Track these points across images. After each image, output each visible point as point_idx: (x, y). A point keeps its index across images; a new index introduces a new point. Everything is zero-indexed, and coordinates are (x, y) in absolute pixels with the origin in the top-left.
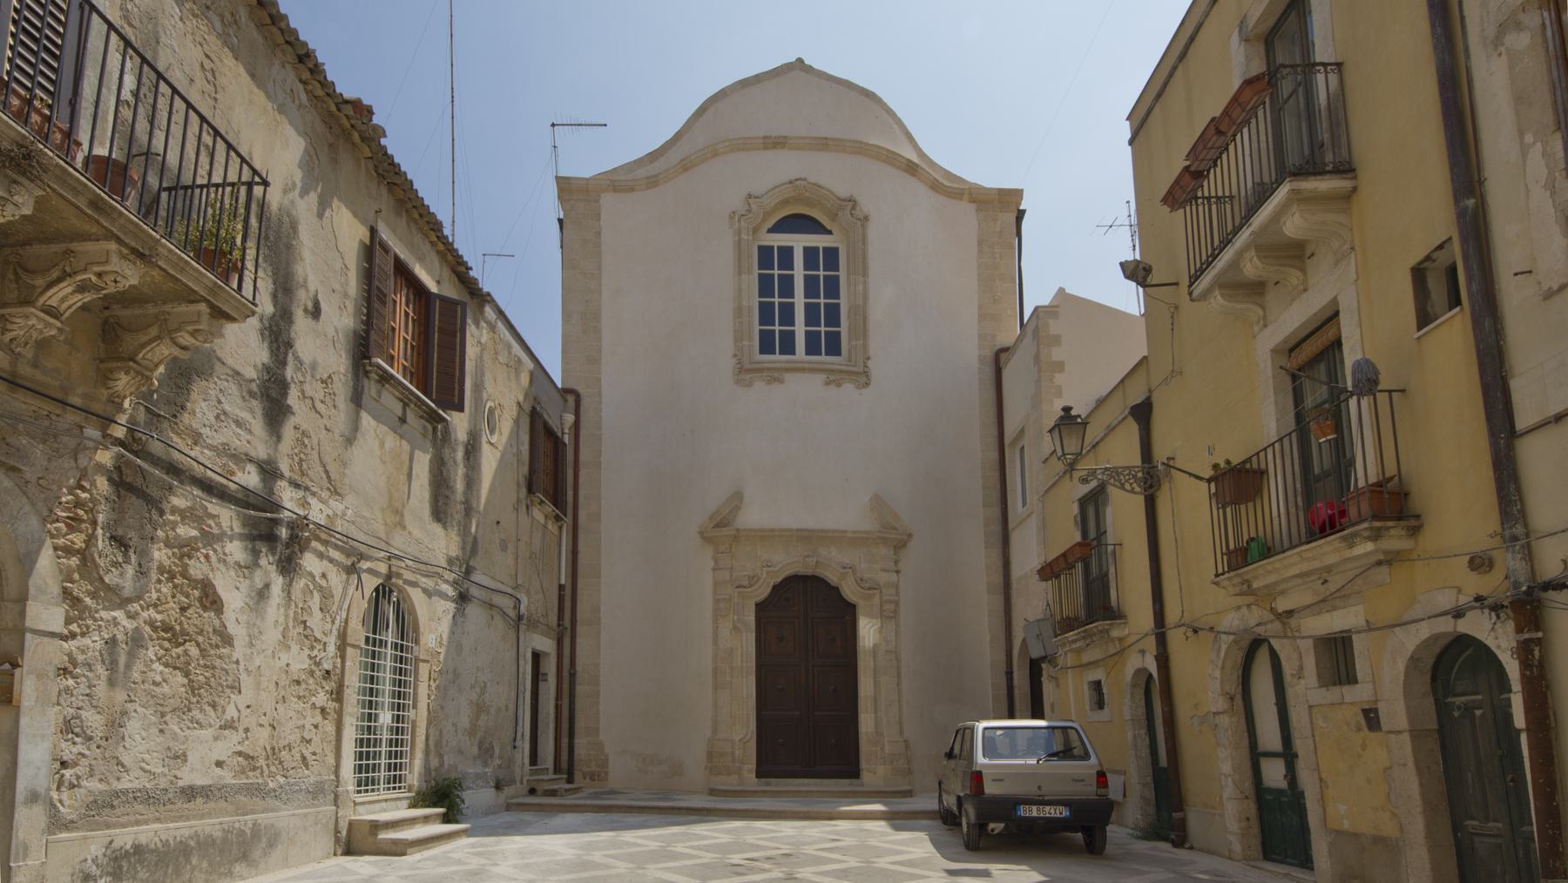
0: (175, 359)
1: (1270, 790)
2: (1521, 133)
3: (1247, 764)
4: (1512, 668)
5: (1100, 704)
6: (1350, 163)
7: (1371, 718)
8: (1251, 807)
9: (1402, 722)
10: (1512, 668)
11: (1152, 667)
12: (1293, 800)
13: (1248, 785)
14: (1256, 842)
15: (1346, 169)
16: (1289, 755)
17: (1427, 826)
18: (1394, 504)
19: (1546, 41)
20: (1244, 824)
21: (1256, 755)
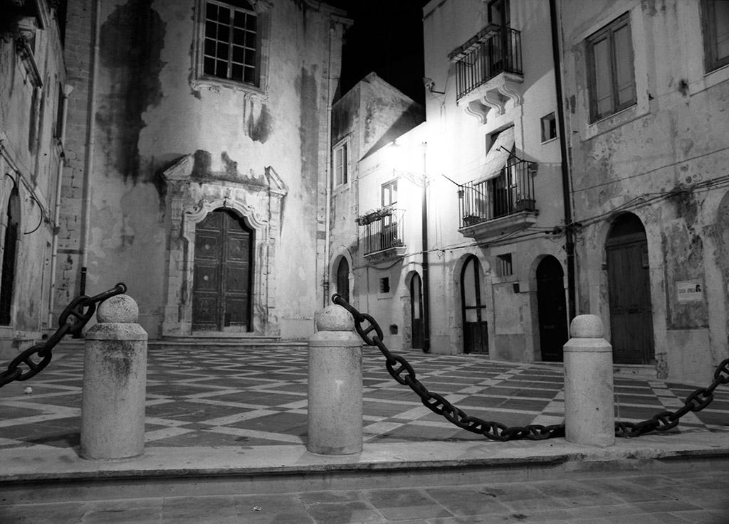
0: (374, 494)
1: (470, 323)
2: (577, 85)
3: (461, 312)
4: (565, 268)
5: (385, 281)
6: (521, 71)
7: (516, 288)
8: (460, 331)
9: (527, 289)
10: (565, 268)
11: (420, 270)
12: (482, 325)
13: (461, 321)
14: (462, 347)
15: (520, 73)
16: (480, 307)
17: (544, 75)
18: (530, 206)
19: (571, 174)
20: (458, 338)
21: (465, 308)
